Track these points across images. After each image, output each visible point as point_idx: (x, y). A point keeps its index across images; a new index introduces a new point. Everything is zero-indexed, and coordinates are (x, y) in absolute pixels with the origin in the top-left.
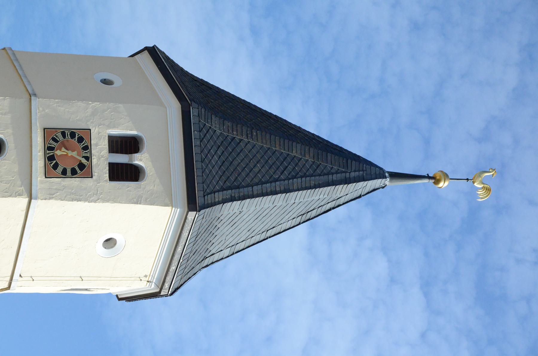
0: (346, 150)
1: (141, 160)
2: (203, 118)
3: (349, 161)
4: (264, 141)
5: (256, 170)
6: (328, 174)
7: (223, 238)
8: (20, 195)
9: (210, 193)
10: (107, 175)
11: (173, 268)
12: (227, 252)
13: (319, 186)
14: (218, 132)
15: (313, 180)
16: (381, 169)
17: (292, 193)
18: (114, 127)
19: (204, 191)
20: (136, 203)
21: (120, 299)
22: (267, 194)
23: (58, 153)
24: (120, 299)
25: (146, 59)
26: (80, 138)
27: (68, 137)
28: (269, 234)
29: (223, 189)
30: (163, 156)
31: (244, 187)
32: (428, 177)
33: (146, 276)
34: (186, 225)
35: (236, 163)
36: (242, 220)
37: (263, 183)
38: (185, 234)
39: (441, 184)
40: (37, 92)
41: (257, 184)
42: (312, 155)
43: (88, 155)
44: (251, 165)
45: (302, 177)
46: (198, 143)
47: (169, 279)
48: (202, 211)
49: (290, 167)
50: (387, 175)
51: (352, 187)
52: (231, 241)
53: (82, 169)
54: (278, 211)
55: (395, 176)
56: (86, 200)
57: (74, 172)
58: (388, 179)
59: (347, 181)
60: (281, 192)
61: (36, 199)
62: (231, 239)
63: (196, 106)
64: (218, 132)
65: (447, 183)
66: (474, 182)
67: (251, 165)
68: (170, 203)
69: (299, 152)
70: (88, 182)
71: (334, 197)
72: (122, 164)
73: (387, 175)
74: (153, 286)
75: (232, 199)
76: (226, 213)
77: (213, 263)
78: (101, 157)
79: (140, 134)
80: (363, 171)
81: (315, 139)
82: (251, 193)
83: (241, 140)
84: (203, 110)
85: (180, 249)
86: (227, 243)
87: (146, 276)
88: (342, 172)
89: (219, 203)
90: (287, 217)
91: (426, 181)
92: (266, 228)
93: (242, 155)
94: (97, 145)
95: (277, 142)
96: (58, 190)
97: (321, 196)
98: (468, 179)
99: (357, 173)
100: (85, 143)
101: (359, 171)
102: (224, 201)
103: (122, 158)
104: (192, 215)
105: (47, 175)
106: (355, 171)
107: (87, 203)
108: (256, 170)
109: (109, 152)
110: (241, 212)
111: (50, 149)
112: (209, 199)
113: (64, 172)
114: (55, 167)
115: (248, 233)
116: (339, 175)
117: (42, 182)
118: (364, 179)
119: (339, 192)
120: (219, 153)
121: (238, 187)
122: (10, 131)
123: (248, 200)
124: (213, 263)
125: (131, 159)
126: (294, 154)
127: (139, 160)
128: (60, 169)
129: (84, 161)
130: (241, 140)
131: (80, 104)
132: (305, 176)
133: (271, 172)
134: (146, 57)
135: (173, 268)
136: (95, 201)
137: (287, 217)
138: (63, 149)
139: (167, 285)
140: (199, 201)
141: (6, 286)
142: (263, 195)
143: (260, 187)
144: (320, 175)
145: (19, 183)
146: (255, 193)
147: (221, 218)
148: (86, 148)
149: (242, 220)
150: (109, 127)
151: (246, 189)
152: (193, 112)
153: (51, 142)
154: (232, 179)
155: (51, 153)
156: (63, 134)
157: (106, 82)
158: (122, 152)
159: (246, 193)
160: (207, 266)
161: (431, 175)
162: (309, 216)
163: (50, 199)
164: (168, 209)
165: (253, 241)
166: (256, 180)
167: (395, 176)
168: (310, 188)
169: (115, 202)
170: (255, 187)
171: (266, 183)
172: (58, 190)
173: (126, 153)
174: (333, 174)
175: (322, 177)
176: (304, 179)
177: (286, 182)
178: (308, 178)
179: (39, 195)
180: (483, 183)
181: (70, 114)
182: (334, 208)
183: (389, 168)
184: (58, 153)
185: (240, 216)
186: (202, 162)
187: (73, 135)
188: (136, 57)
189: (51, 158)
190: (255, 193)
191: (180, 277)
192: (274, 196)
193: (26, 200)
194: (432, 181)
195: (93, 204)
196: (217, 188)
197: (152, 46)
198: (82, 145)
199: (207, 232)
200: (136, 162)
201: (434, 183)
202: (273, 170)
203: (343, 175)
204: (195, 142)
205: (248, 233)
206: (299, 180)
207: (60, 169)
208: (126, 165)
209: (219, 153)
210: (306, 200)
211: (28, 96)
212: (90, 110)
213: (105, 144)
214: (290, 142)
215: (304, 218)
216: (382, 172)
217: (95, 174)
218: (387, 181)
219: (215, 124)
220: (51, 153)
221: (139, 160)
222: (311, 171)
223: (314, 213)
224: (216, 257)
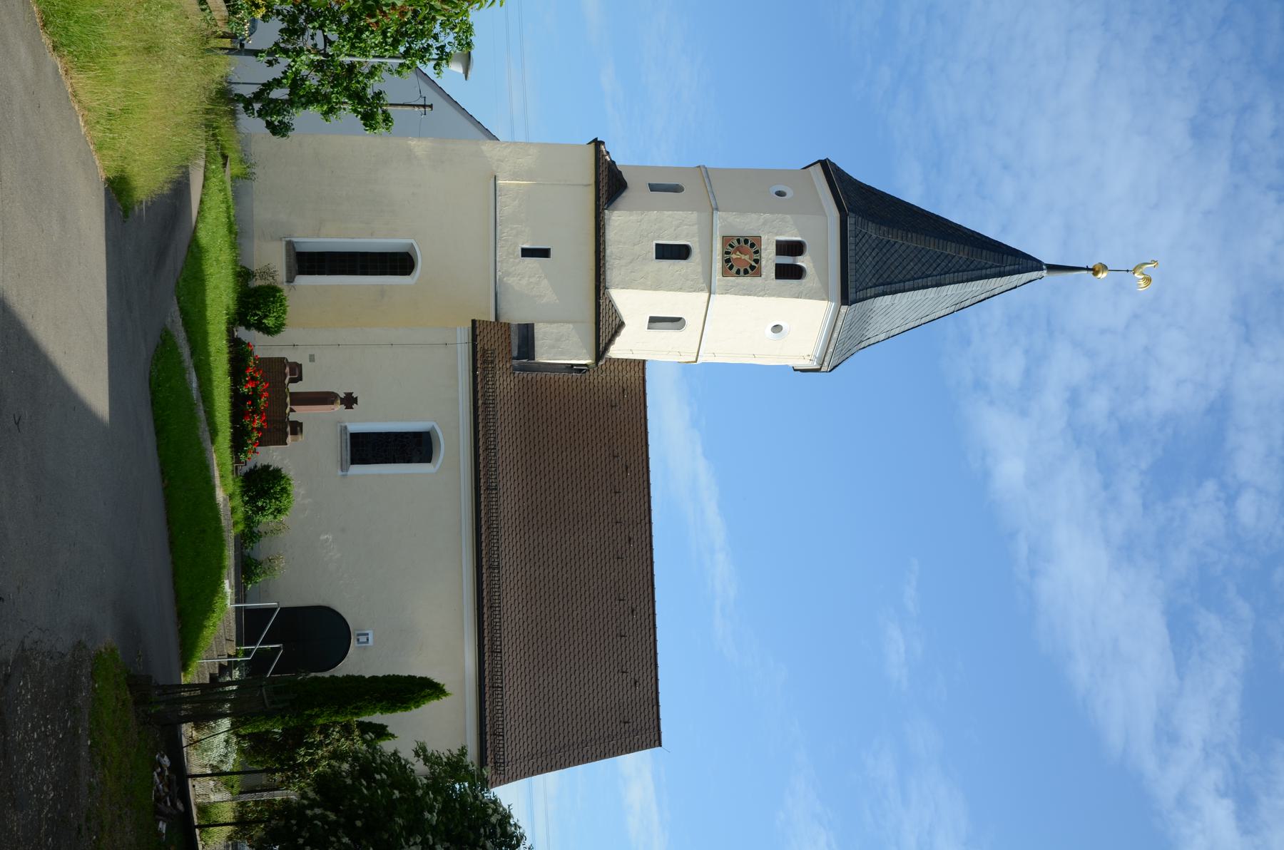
30: (821, 260)
32: (1088, 269)
53: (753, 269)
78: (769, 259)
105: (724, 274)
127: (801, 261)
167: (1053, 268)
183: (1047, 260)
221: (801, 261)
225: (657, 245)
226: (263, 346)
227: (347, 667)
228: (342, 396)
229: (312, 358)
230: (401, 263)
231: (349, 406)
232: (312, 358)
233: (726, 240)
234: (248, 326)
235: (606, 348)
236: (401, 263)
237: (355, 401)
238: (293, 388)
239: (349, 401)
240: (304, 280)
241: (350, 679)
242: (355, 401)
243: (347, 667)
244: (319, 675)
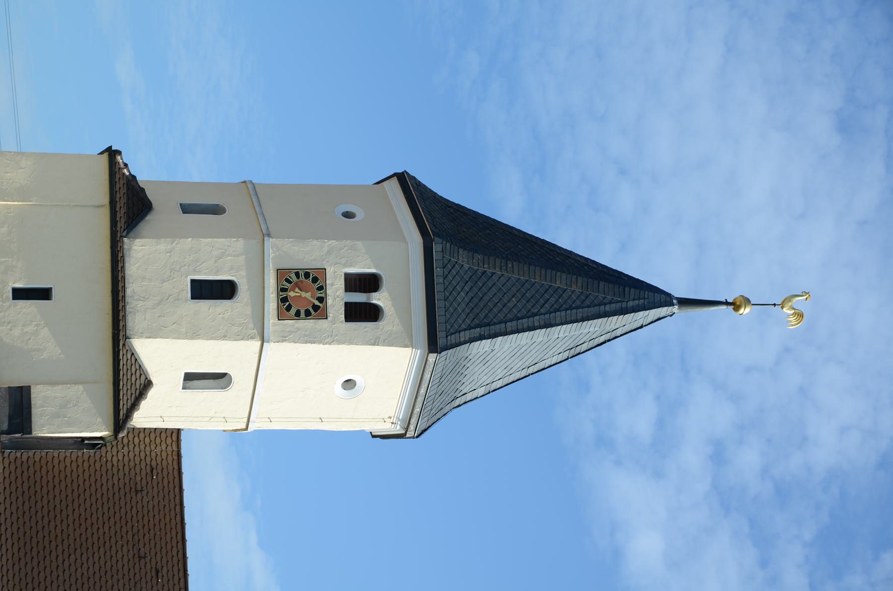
0: (627, 276)
1: (379, 299)
2: (448, 253)
3: (627, 289)
4: (521, 273)
5: (511, 305)
6: (599, 305)
7: (475, 376)
8: (252, 338)
9: (455, 333)
10: (343, 316)
11: (417, 410)
12: (481, 391)
13: (588, 318)
14: (466, 266)
15: (580, 313)
16: (669, 295)
17: (553, 328)
18: (351, 266)
19: (447, 331)
20: (374, 344)
21: (374, 436)
22: (524, 330)
23: (292, 294)
24: (374, 436)
25: (394, 189)
26: (314, 278)
27: (302, 278)
28: (531, 370)
29: (470, 328)
30: (403, 295)
31: (495, 324)
32: (727, 303)
33: (390, 418)
34: (427, 367)
35: (486, 298)
36: (495, 358)
37: (518, 319)
38: (427, 376)
39: (742, 311)
40: (272, 230)
41: (511, 320)
42: (579, 284)
43: (323, 295)
44: (505, 300)
45: (566, 310)
46: (441, 280)
47: (414, 421)
48: (443, 353)
49: (552, 300)
50: (675, 301)
51: (629, 317)
52: (485, 379)
53: (317, 310)
54: (539, 347)
55: (685, 302)
56: (320, 342)
57: (308, 314)
58: (676, 307)
59: (623, 312)
60: (540, 327)
61: (268, 342)
62: (485, 378)
63: (439, 240)
64: (466, 266)
65: (748, 310)
66: (782, 308)
67: (505, 300)
68: (410, 344)
69: (564, 282)
70: (322, 323)
71: (608, 329)
73: (675, 301)
74: (398, 427)
75: (481, 338)
76: (474, 352)
77: (465, 403)
78: (337, 296)
80: (644, 298)
81: (587, 265)
82: (503, 330)
83: (493, 274)
84: (448, 245)
85: (423, 391)
86: (481, 382)
87: (390, 418)
88: (619, 302)
89: (465, 343)
90: (551, 352)
91: (724, 307)
92: (527, 364)
93: (494, 289)
94: (332, 285)
95: (538, 273)
96: (291, 332)
98: (775, 305)
99: (637, 302)
100: (319, 283)
101: (639, 299)
102: (472, 340)
103: (359, 298)
104: (432, 357)
105: (280, 317)
106: (634, 300)
107: (321, 345)
108: (511, 305)
109: (346, 291)
110: (492, 351)
111: (284, 290)
112: (453, 339)
113: (321, 300)
114: (289, 308)
115: (505, 371)
116: (613, 305)
117: (274, 325)
118: (645, 308)
120: (467, 288)
121: (489, 325)
122: (243, 273)
123: (500, 338)
124: (465, 403)
125: (369, 298)
126: (558, 284)
127: (377, 299)
128: (293, 311)
129: (317, 303)
130: (493, 274)
131: (315, 242)
132: (571, 308)
133: (529, 306)
134: (395, 183)
135: (417, 410)
136: (330, 344)
137: (551, 352)
138: (297, 290)
139: (412, 427)
140: (441, 342)
141: (244, 427)
142: (518, 331)
143: (514, 323)
144: (589, 307)
145: (251, 325)
146: (509, 329)
147: (470, 357)
148: (321, 288)
149: (495, 358)
150: (345, 266)
151: (498, 326)
152: (436, 248)
154: (482, 316)
155: (284, 294)
156: (297, 274)
157: (348, 215)
159: (498, 331)
160: (459, 406)
161: (730, 300)
162: (578, 350)
163: (283, 341)
164: (408, 352)
165: (511, 379)
166: (510, 316)
167: (685, 302)
168: (577, 321)
169: (351, 344)
170: (509, 324)
171: (522, 318)
172: (291, 332)
173: (365, 292)
174: (605, 304)
175: (592, 309)
176: (569, 312)
177: (547, 316)
178: (574, 311)
179: (271, 338)
180: (794, 309)
181: (304, 254)
182: (609, 340)
183: (678, 292)
184: (292, 294)
185: (492, 354)
186: (445, 300)
187: (307, 275)
188: (384, 183)
189: (284, 300)
190: (509, 329)
191: (426, 419)
192: (532, 332)
193: (260, 342)
194: (731, 308)
195: (327, 346)
196: (464, 326)
197: (401, 171)
198: (316, 286)
199: (458, 370)
200: (374, 302)
201: (734, 309)
202: (531, 304)
203: (619, 305)
204: (438, 280)
205: (505, 371)
206: (563, 313)
207: (293, 311)
208: (365, 303)
209: (467, 288)
210: (572, 334)
211: (261, 236)
212: (326, 249)
213: (341, 283)
214: (554, 272)
215: (572, 352)
216: (668, 299)
217: (330, 315)
218: (675, 309)
219: (463, 259)
220: (284, 294)
221: (377, 299)
222: (578, 303)
223: (584, 347)
224: (469, 397)
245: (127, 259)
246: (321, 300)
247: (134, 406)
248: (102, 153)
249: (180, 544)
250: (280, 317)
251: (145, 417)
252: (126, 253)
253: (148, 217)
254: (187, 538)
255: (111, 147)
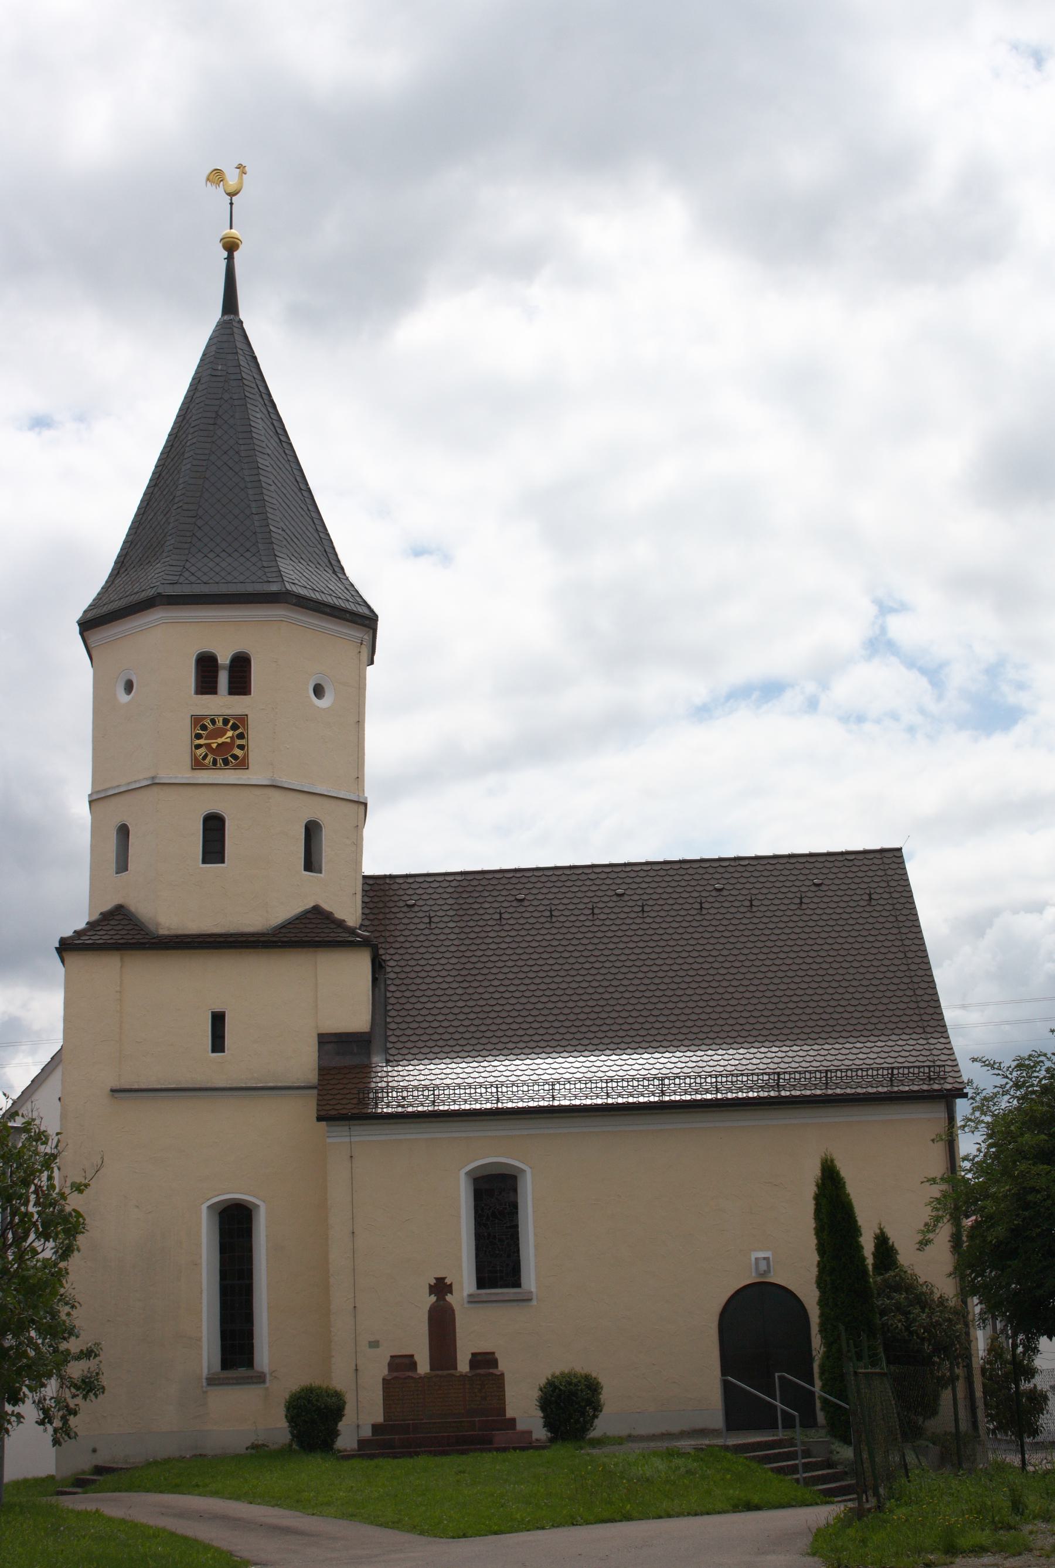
30: (223, 634)
32: (230, 259)
43: (221, 719)
53: (238, 724)
72: (230, 682)
78: (221, 704)
79: (462, 1173)
97: (258, 416)
98: (231, 204)
103: (223, 679)
105: (243, 764)
119: (253, 391)
127: (224, 659)
153: (206, 761)
158: (216, 682)
167: (230, 304)
173: (217, 672)
183: (215, 314)
197: (78, 628)
211: (155, 789)
221: (224, 659)
225: (223, 1051)
226: (363, 1413)
227: (807, 1290)
228: (433, 1298)
229: (374, 1344)
230: (235, 1224)
231: (449, 1289)
232: (374, 1344)
233: (197, 764)
234: (334, 1434)
235: (352, 931)
236: (235, 1224)
237: (440, 1280)
238: (423, 1367)
239: (441, 1288)
240: (264, 1354)
241: (820, 1283)
242: (440, 1280)
243: (807, 1290)
244: (815, 1329)
245: (180, 932)
246: (226, 722)
247: (340, 924)
248: (63, 962)
249: (487, 876)
250: (243, 764)
251: (349, 910)
252: (173, 932)
253: (133, 909)
254: (825, 851)
255: (57, 948)
